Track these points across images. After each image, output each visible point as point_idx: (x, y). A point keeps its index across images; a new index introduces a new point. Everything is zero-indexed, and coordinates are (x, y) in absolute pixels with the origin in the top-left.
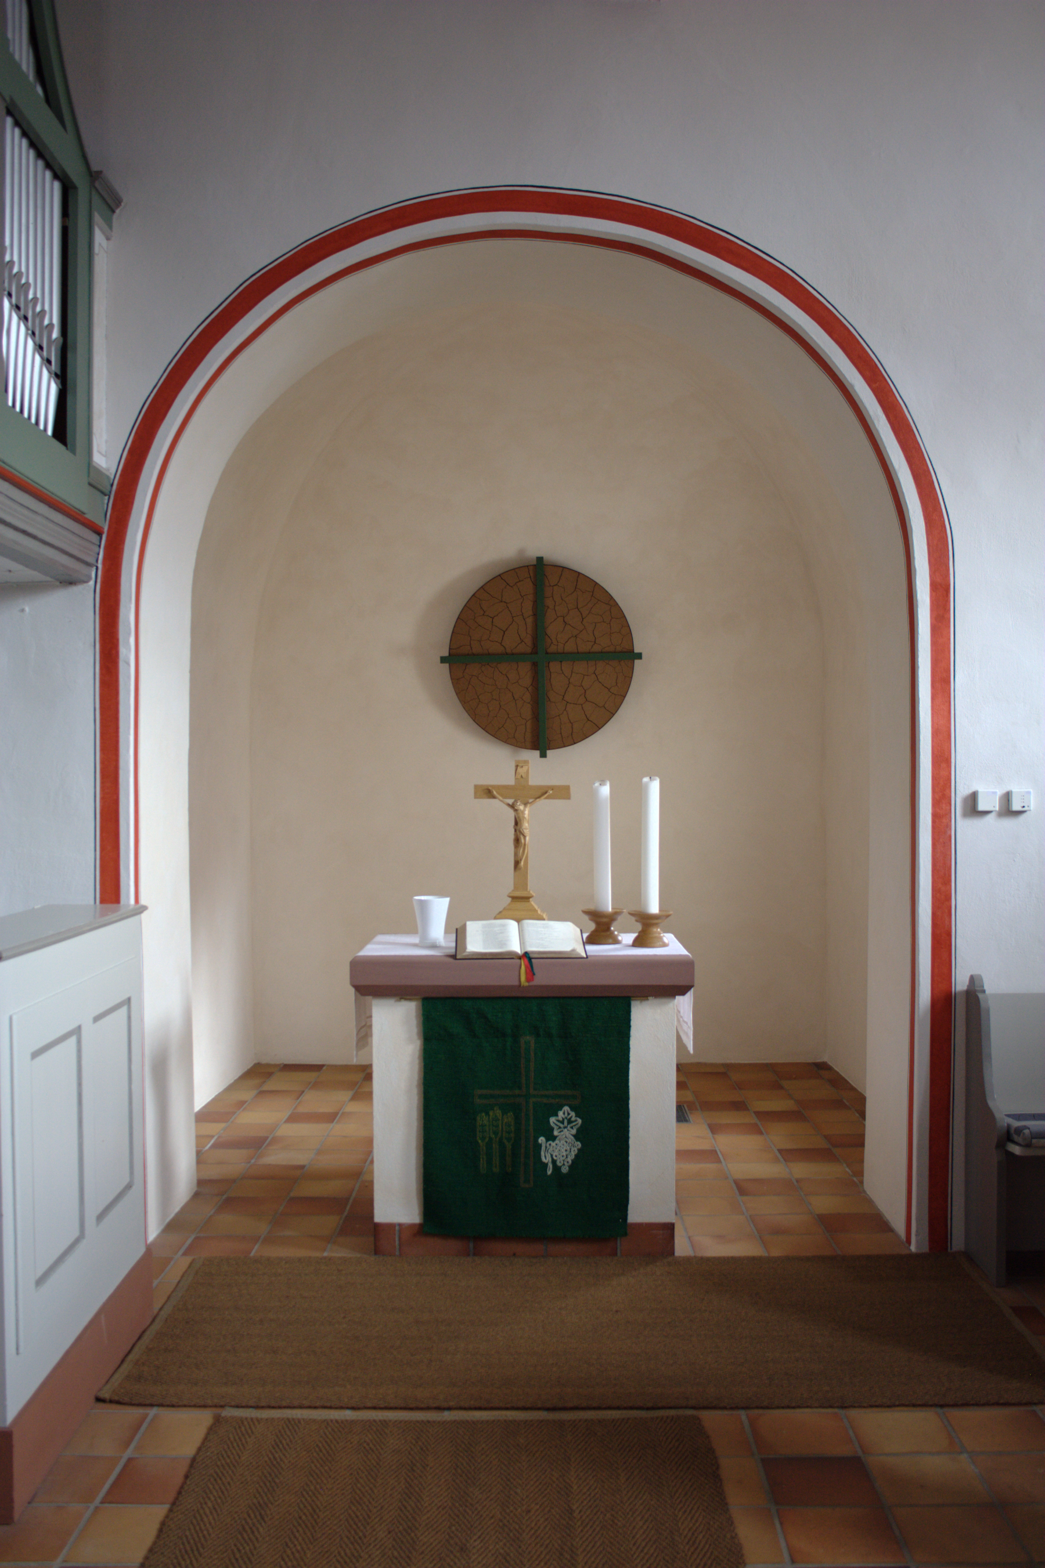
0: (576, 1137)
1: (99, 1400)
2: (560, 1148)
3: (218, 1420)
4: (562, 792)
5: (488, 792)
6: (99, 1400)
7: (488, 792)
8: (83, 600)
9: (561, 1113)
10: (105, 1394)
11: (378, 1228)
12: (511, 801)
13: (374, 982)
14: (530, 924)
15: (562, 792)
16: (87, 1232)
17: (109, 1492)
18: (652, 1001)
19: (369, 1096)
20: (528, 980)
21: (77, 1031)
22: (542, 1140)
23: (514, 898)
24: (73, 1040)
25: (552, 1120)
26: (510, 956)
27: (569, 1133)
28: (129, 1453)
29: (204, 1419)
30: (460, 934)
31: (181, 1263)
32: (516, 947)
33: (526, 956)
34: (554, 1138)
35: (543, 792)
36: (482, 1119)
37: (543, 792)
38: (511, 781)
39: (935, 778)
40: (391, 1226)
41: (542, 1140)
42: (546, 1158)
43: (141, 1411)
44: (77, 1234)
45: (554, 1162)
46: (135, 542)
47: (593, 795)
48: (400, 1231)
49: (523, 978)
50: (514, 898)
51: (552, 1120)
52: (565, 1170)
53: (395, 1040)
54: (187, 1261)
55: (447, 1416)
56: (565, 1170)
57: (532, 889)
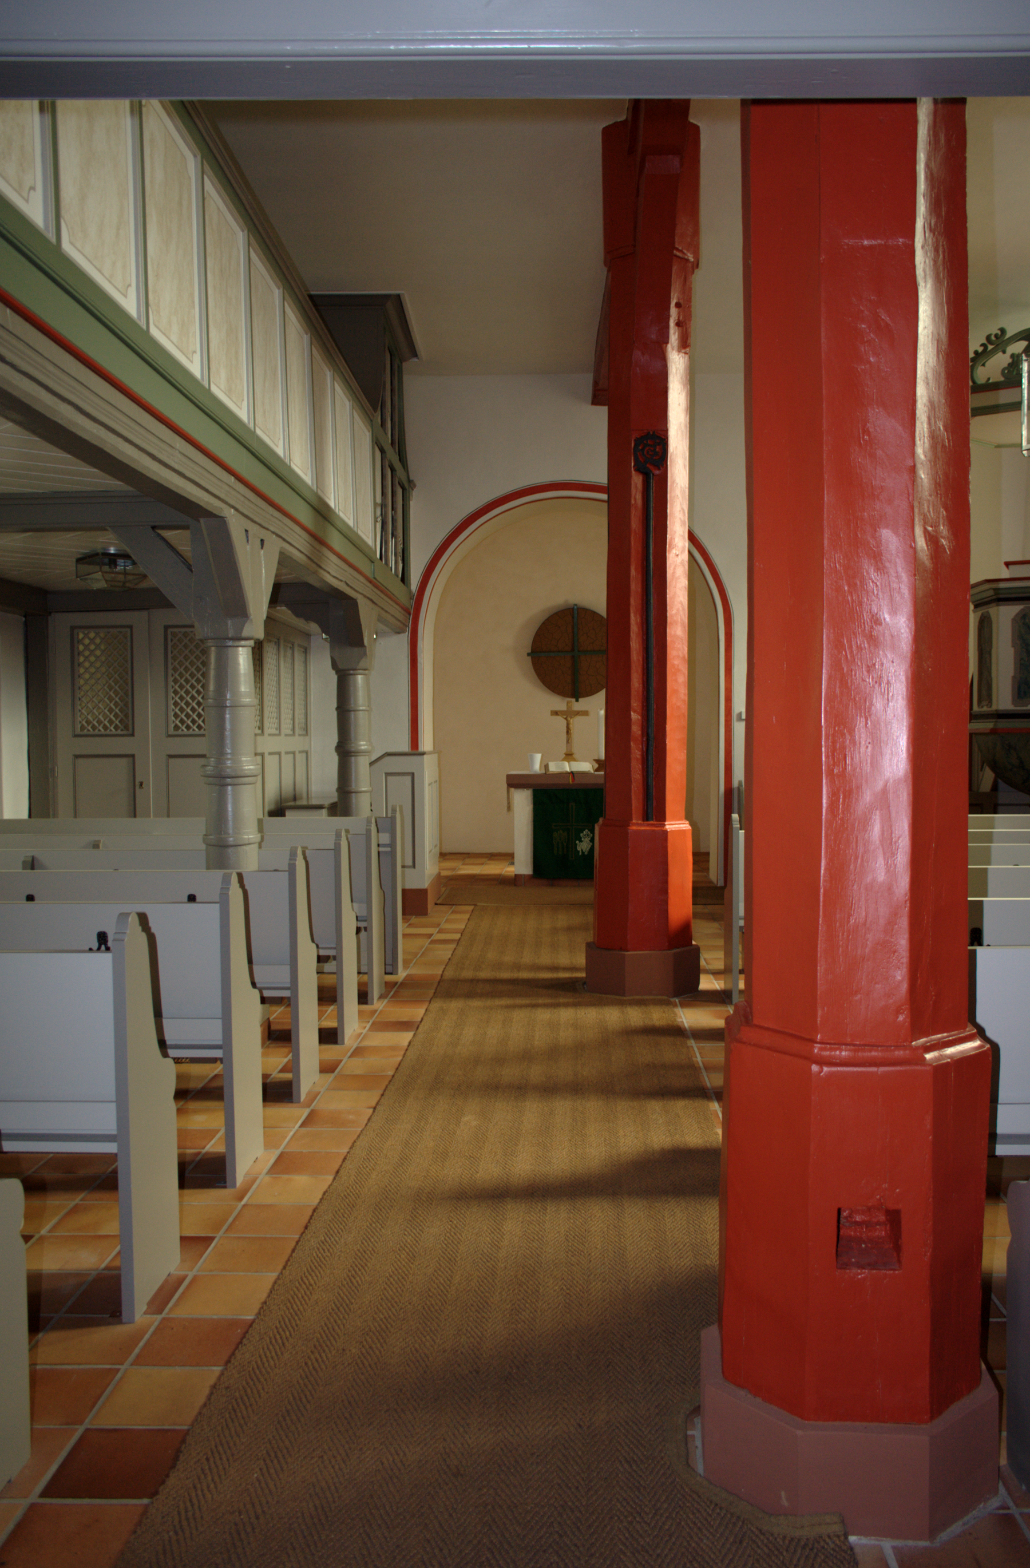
4: (585, 713)
5: (555, 713)
7: (555, 713)
8: (405, 638)
13: (515, 782)
14: (573, 763)
15: (585, 713)
19: (178, 1130)
26: (567, 773)
30: (546, 767)
32: (568, 770)
33: (572, 773)
35: (578, 713)
36: (555, 835)
37: (578, 713)
39: (726, 721)
42: (579, 849)
47: (598, 714)
48: (698, 871)
53: (523, 802)
57: (575, 750)
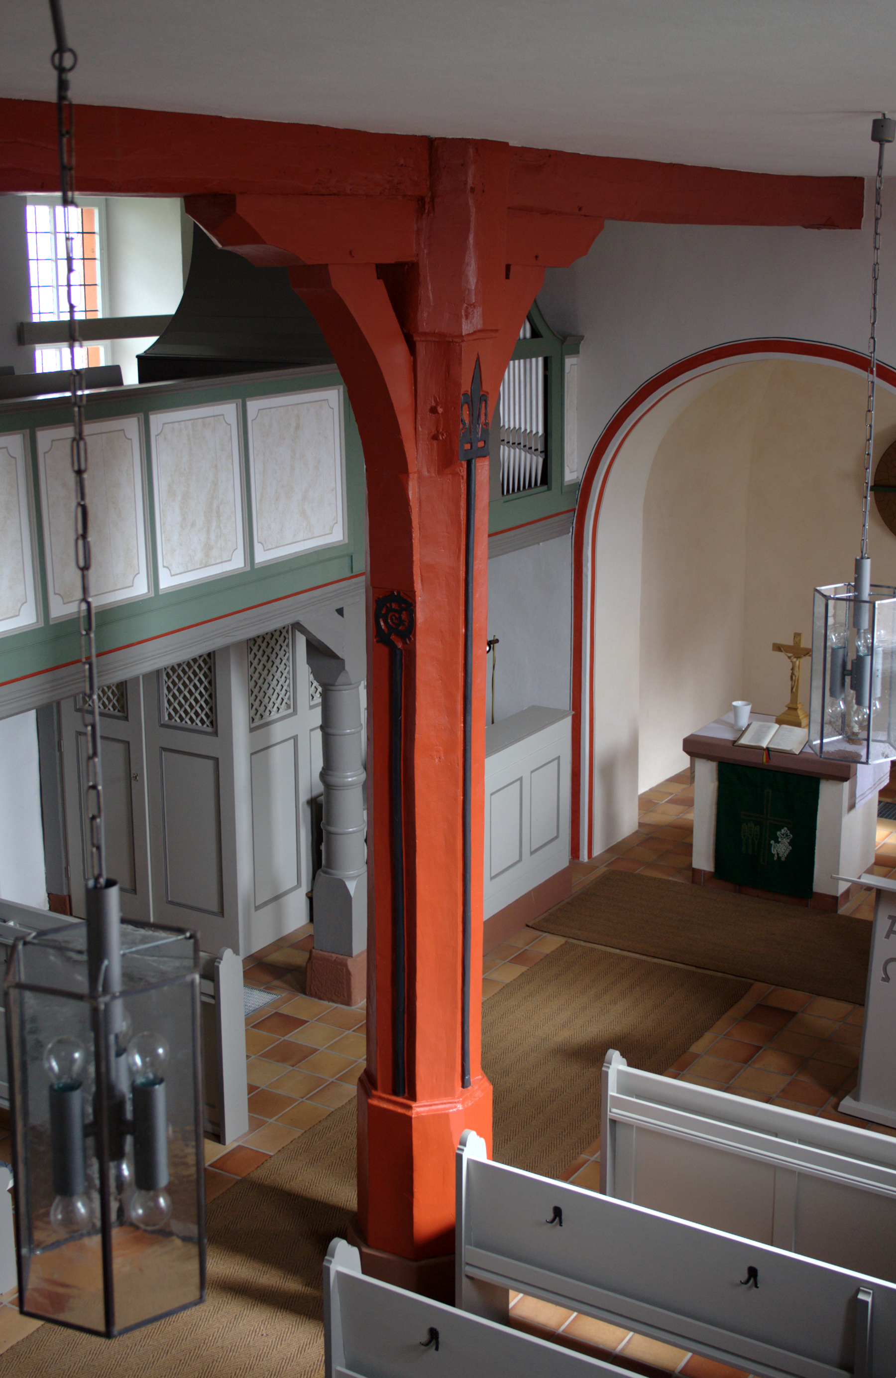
0: (790, 844)
1: (527, 926)
2: (781, 848)
3: (566, 942)
5: (778, 648)
6: (527, 926)
7: (778, 648)
8: (567, 541)
9: (783, 831)
10: (530, 924)
11: (694, 870)
12: (790, 655)
16: (523, 858)
17: (65, 913)
18: (830, 781)
20: (767, 761)
21: (521, 779)
22: (772, 842)
23: (789, 708)
24: (518, 782)
25: (778, 833)
26: (761, 748)
27: (786, 841)
28: (527, 948)
29: (562, 940)
31: (602, 869)
34: (779, 842)
38: (791, 643)
40: (700, 871)
41: (772, 842)
42: (774, 851)
43: (541, 933)
44: (518, 859)
45: (778, 854)
46: (170, 1119)
49: (765, 760)
50: (789, 708)
51: (778, 833)
52: (783, 859)
54: (605, 869)
55: (655, 960)
56: (783, 859)
